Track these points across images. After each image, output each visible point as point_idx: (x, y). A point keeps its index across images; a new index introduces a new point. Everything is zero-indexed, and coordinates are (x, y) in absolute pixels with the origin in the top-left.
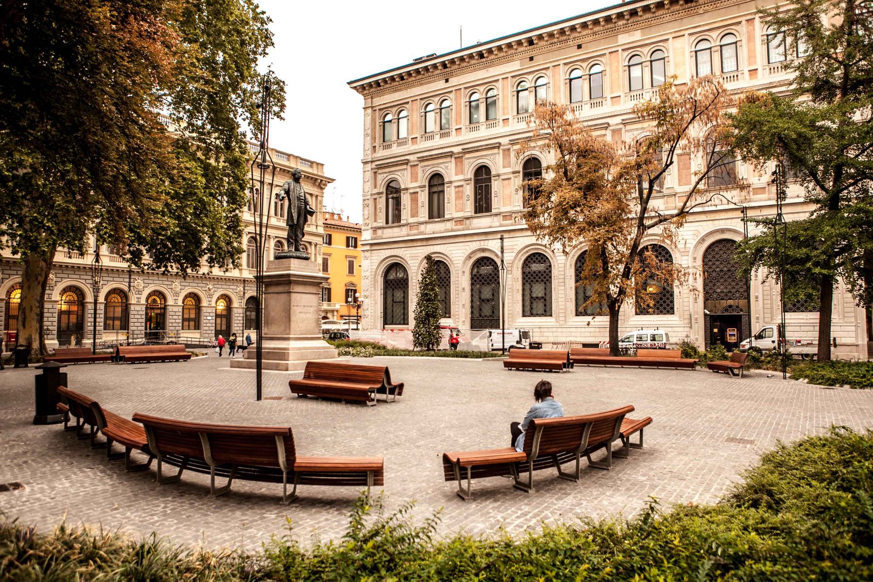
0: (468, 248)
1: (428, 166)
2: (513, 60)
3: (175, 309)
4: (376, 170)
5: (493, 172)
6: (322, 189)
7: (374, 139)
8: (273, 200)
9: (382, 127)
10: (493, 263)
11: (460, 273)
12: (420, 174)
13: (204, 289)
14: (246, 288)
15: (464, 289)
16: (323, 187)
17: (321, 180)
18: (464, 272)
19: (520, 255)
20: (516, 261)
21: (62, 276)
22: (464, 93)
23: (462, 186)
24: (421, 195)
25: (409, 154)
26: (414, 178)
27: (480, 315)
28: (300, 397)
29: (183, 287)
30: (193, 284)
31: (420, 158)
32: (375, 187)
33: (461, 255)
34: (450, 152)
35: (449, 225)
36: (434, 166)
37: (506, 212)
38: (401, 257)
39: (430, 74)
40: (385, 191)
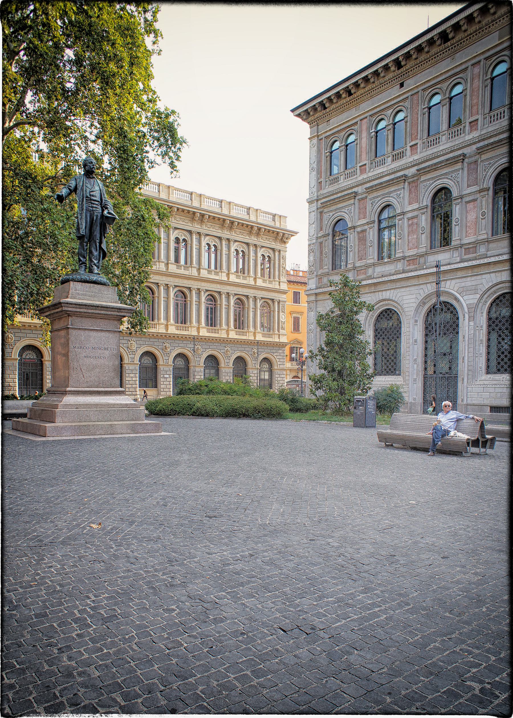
0: (421, 292)
1: (377, 197)
2: (489, 33)
3: (227, 370)
4: (322, 210)
5: (455, 193)
6: (285, 243)
7: (319, 173)
8: (172, 245)
9: (328, 158)
10: (452, 309)
11: (412, 321)
12: (369, 208)
13: (250, 352)
14: (260, 350)
15: (416, 341)
16: (285, 240)
17: (284, 234)
18: (416, 321)
19: (486, 296)
20: (480, 305)
21: (20, 335)
22: (423, 96)
23: (416, 217)
24: (369, 233)
25: (357, 186)
26: (362, 213)
27: (435, 372)
28: (387, 446)
29: (17, 339)
30: (32, 335)
31: (369, 188)
32: (321, 229)
33: (414, 300)
34: (402, 176)
35: (400, 266)
36: (384, 196)
37: (469, 244)
38: (396, 302)
39: (381, 80)
40: (331, 233)
